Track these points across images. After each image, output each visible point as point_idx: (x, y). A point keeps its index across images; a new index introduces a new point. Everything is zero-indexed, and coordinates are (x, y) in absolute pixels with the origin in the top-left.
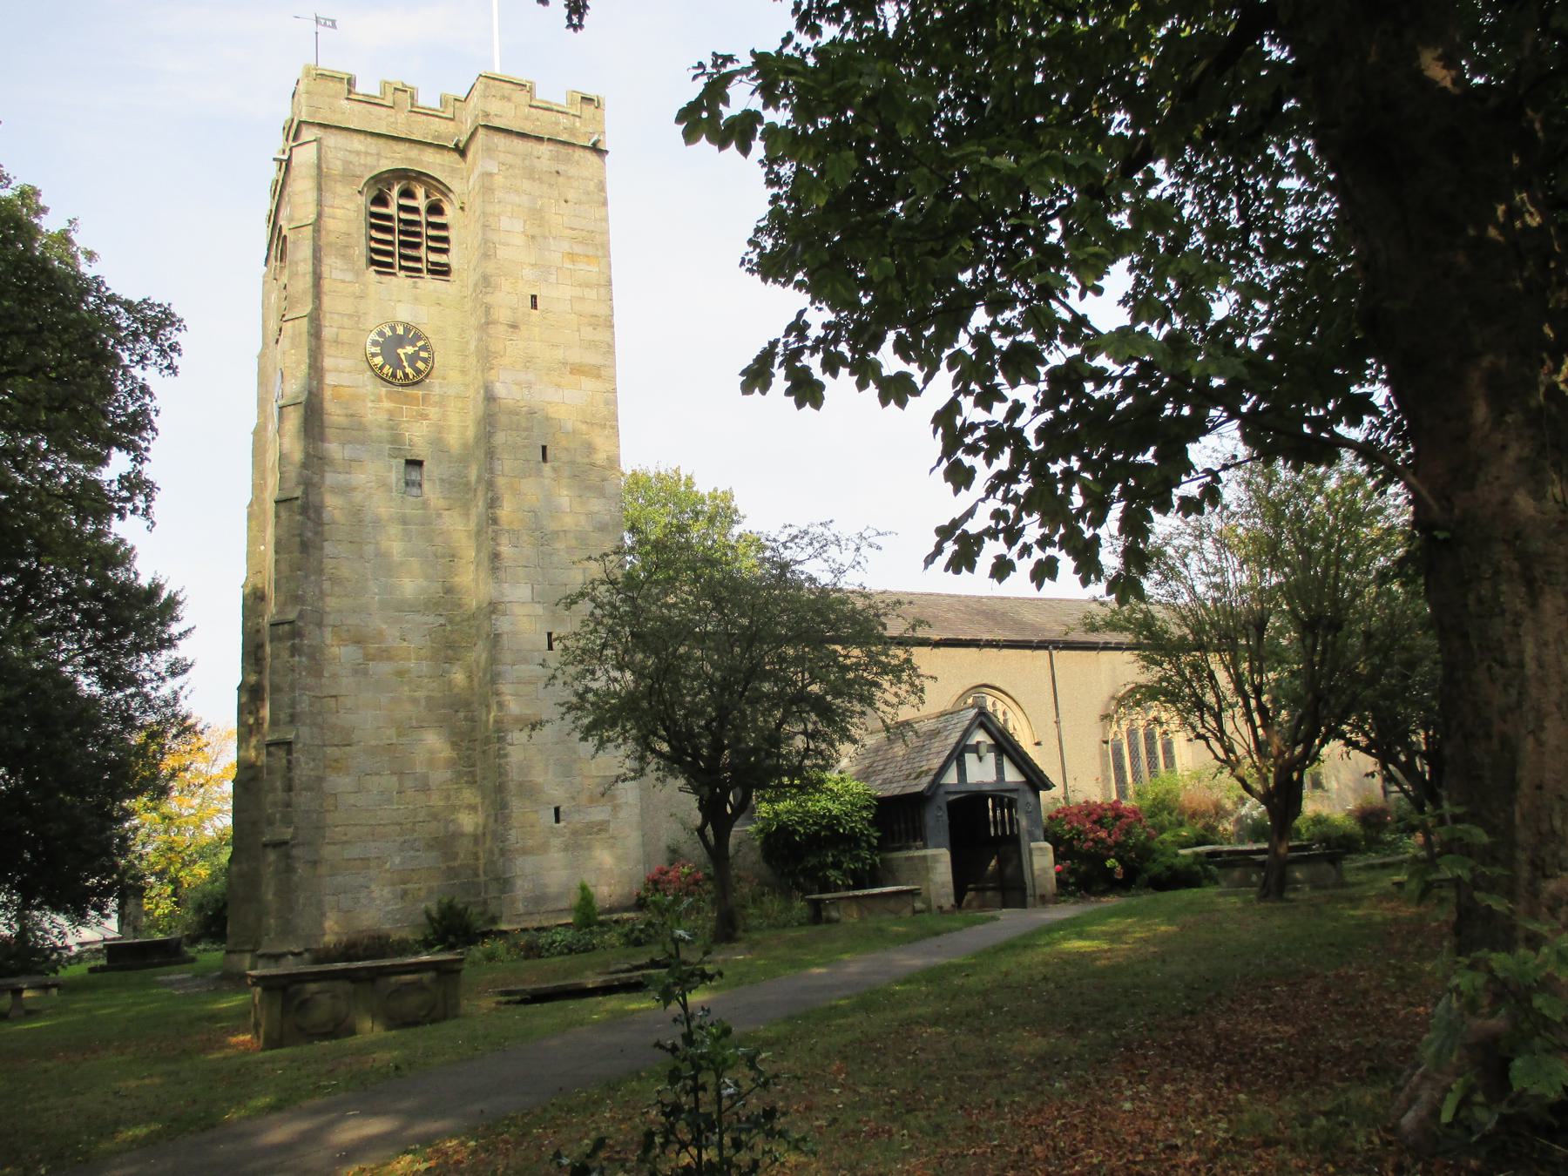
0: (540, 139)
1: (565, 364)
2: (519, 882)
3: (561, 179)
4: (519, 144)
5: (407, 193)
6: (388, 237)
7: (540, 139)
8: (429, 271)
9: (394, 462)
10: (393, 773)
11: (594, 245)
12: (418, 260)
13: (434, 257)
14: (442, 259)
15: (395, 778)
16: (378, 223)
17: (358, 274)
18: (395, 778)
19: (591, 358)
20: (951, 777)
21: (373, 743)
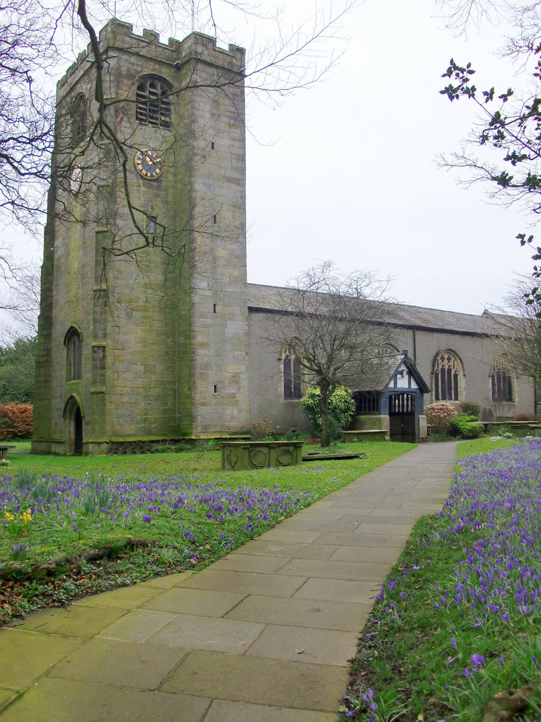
1: (225, 177)
8: (161, 125)
10: (141, 365)
11: (238, 120)
12: (157, 119)
13: (163, 118)
14: (168, 119)
15: (142, 367)
18: (142, 367)
19: (236, 175)
20: (391, 385)
21: (134, 349)
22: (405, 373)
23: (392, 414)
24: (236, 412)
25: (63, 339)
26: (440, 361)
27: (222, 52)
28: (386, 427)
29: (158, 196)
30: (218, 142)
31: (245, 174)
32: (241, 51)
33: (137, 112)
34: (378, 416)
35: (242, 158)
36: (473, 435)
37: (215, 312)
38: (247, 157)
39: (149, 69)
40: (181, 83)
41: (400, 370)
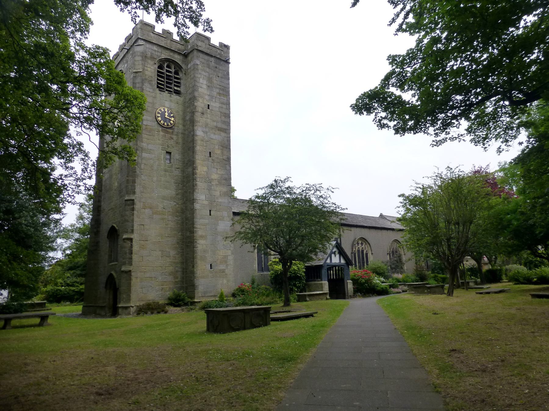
0: (212, 56)
1: (217, 127)
2: (200, 287)
3: (217, 70)
4: (206, 57)
5: (168, 66)
6: (163, 80)
7: (212, 56)
8: (175, 93)
9: (163, 152)
12: (171, 88)
13: (176, 88)
14: (179, 89)
16: (160, 74)
17: (154, 90)
19: (224, 127)
20: (328, 261)
22: (337, 253)
23: (330, 281)
25: (106, 234)
26: (356, 245)
28: (326, 288)
30: (212, 104)
31: (230, 126)
32: (227, 47)
33: (158, 83)
34: (321, 282)
35: (228, 116)
36: (383, 292)
37: (210, 215)
38: (231, 115)
39: (165, 55)
40: (187, 66)
41: (334, 251)
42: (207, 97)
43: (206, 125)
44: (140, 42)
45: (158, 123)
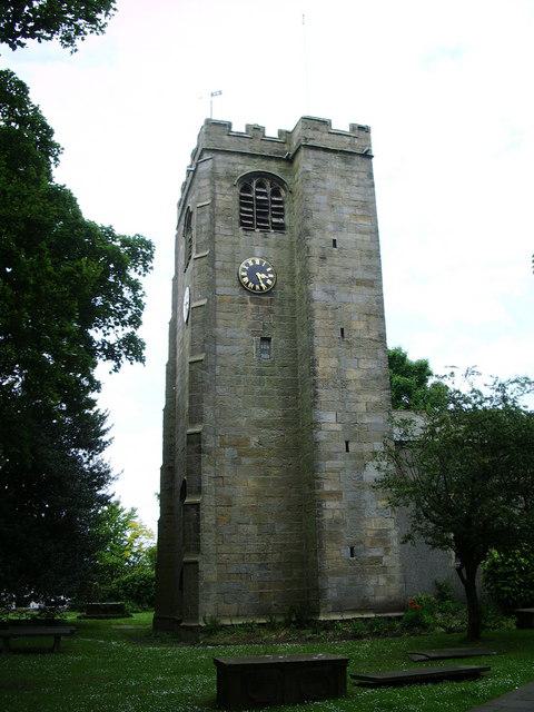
5: (260, 185)
12: (267, 222)
13: (275, 220)
16: (244, 201)
24: (382, 581)
27: (272, 141)
29: (271, 311)
32: (365, 130)
33: (241, 217)
37: (347, 451)
42: (330, 227)
43: (332, 278)
44: (206, 156)
45: (243, 286)
